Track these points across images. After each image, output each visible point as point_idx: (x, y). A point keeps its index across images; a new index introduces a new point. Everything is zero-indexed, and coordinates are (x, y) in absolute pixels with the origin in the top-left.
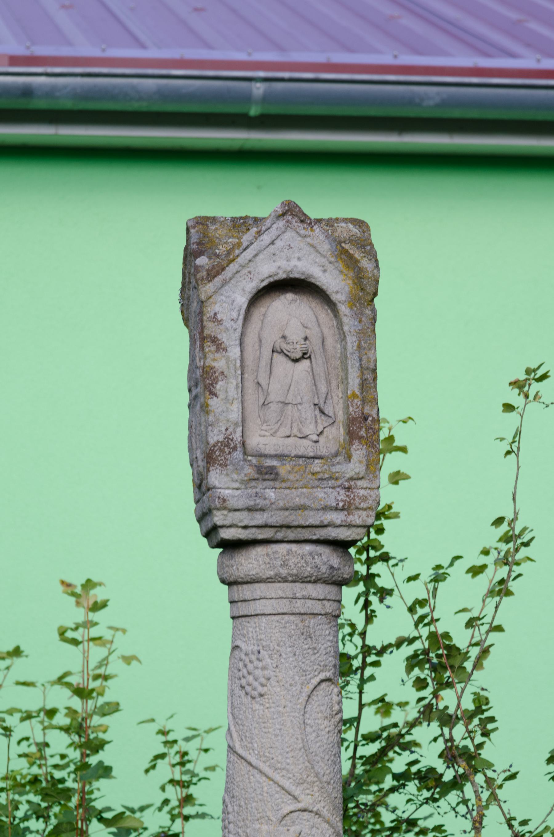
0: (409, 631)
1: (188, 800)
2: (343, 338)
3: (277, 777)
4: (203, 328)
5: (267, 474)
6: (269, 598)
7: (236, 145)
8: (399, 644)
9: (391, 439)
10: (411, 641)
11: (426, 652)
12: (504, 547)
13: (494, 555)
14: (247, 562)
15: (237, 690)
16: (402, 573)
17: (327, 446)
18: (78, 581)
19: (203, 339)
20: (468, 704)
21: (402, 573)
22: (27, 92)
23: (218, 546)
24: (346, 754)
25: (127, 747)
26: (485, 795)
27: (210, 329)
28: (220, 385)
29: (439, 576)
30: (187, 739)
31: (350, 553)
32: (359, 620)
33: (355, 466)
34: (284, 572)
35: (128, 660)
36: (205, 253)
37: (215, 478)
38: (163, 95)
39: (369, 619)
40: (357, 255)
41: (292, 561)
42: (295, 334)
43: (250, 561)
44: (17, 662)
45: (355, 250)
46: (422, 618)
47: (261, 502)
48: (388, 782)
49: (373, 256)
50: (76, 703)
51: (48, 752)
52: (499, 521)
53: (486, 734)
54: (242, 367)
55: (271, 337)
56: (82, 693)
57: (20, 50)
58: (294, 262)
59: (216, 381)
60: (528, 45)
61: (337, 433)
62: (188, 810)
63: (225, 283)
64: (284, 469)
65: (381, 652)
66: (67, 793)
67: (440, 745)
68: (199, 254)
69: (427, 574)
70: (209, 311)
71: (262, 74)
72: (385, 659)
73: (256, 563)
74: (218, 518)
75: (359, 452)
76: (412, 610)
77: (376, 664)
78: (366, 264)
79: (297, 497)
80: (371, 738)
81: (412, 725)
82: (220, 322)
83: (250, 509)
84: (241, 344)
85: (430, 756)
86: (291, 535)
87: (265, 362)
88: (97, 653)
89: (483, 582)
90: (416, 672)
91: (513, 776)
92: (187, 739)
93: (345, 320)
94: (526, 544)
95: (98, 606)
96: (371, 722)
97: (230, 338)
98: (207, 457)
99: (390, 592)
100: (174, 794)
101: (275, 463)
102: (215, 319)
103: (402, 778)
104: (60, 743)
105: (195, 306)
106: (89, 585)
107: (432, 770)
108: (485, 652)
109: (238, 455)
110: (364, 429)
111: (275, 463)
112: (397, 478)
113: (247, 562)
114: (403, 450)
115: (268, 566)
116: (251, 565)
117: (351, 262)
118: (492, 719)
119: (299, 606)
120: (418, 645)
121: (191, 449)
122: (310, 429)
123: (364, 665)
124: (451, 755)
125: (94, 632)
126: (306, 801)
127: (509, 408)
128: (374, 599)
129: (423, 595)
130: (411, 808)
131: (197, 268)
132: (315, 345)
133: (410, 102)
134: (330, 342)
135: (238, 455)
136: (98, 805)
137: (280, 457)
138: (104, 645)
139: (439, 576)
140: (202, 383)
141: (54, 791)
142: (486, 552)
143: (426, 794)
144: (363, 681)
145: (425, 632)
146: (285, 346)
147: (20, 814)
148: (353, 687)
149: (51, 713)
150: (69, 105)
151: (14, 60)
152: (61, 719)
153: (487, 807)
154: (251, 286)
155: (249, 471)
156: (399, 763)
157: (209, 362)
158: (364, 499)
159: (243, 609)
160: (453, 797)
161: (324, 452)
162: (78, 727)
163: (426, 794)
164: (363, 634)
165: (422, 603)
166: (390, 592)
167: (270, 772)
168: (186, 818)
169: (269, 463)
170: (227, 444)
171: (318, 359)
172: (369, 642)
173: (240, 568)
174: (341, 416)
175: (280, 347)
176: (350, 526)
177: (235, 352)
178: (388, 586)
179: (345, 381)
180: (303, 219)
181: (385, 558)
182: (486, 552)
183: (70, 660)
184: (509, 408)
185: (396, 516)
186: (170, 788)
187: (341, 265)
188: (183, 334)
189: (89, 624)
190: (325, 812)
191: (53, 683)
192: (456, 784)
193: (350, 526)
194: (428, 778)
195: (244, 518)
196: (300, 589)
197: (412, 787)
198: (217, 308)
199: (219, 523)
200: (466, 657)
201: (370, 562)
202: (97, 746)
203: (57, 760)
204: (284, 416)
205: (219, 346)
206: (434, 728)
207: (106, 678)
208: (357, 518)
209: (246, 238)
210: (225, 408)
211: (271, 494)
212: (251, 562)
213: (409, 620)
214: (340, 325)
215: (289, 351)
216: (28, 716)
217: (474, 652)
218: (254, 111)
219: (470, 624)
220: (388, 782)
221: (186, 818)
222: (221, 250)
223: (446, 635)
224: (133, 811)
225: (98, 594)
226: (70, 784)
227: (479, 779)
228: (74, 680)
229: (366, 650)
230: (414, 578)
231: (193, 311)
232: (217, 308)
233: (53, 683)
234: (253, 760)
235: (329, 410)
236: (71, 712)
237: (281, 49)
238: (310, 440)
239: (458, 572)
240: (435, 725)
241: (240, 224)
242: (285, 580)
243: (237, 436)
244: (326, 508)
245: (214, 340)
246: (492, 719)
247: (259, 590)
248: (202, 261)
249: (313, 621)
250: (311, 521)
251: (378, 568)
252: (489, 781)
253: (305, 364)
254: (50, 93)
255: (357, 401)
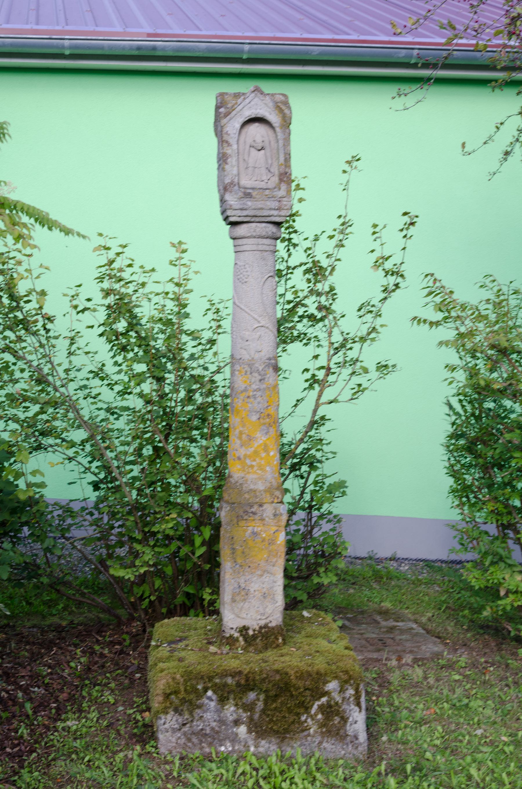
0: (305, 260)
1: (219, 326)
2: (277, 141)
3: (252, 314)
4: (222, 137)
5: (248, 195)
6: (249, 244)
7: (238, 71)
8: (301, 265)
9: (298, 185)
10: (306, 264)
11: (311, 268)
12: (341, 227)
13: (338, 231)
15: (237, 281)
16: (302, 237)
17: (271, 185)
18: (176, 242)
19: (223, 141)
20: (327, 289)
21: (302, 237)
22: (154, 48)
23: (228, 224)
24: (279, 308)
25: (196, 306)
26: (333, 324)
27: (225, 137)
28: (229, 160)
29: (316, 239)
30: (219, 303)
31: (281, 225)
32: (286, 256)
33: (282, 192)
34: (254, 234)
35: (196, 273)
36: (222, 109)
37: (227, 197)
38: (209, 50)
39: (289, 255)
40: (283, 107)
41: (258, 230)
42: (259, 139)
44: (154, 274)
45: (283, 108)
46: (309, 255)
47: (245, 207)
48: (296, 319)
49: (289, 108)
50: (176, 289)
51: (166, 308)
52: (340, 217)
53: (334, 300)
54: (238, 153)
55: (249, 141)
56: (178, 285)
57: (151, 31)
58: (258, 111)
59: (227, 158)
60: (355, 30)
61: (276, 179)
62: (220, 331)
63: (231, 119)
64: (254, 193)
65: (294, 268)
66: (173, 324)
67: (316, 305)
68: (221, 107)
69: (312, 238)
70: (225, 130)
71: (248, 41)
72: (295, 271)
74: (229, 213)
75: (283, 187)
76: (305, 251)
77: (292, 273)
78: (286, 111)
79: (259, 205)
80: (289, 302)
81: (306, 297)
82: (229, 135)
83: (241, 209)
84: (238, 143)
85: (312, 309)
86: (257, 219)
87: (247, 150)
88: (184, 270)
89: (334, 242)
90: (307, 276)
91: (343, 316)
92: (219, 303)
93: (279, 134)
94: (350, 226)
95: (184, 251)
96: (289, 296)
97: (233, 141)
98: (224, 188)
99: (297, 245)
100: (214, 324)
101: (250, 191)
102: (227, 133)
103: (302, 317)
104: (170, 305)
105: (219, 129)
106: (180, 243)
107: (312, 314)
108: (333, 269)
109: (236, 188)
110: (285, 177)
111: (250, 191)
112: (301, 200)
114: (303, 189)
117: (281, 111)
118: (335, 294)
119: (260, 247)
120: (308, 266)
121: (218, 186)
122: (264, 178)
123: (287, 274)
124: (320, 308)
125: (183, 262)
126: (263, 323)
127: (344, 172)
128: (291, 248)
129: (309, 246)
130: (305, 329)
131: (220, 113)
132: (266, 144)
133: (307, 53)
134: (273, 143)
135: (236, 188)
136: (185, 328)
137: (253, 189)
138: (187, 267)
139: (316, 239)
140: (222, 159)
141: (169, 323)
142: (335, 230)
143: (311, 323)
144: (287, 280)
145: (311, 260)
146: (255, 145)
147: (155, 332)
148: (283, 282)
149: (167, 293)
150: (171, 54)
151: (149, 35)
152: (171, 296)
153: (333, 327)
154: (242, 120)
155: (241, 194)
156: (301, 311)
157: (225, 151)
158: (286, 205)
159: (239, 249)
160: (321, 324)
161: (270, 187)
162: (177, 299)
163: (311, 323)
164: (287, 261)
165: (310, 249)
166: (297, 245)
167: (249, 312)
168: (219, 334)
169: (248, 191)
170: (232, 183)
171: (268, 150)
172: (290, 264)
174: (277, 173)
176: (280, 216)
177: (235, 147)
178: (297, 242)
179: (278, 158)
180: (262, 93)
181: (296, 232)
182: (335, 230)
183: (174, 272)
184: (344, 172)
185: (300, 215)
186: (212, 322)
187: (277, 112)
188: (214, 141)
189: (181, 258)
190: (270, 327)
191: (168, 282)
192: (322, 319)
193: (280, 216)
194: (311, 317)
195: (239, 213)
196: (261, 241)
197: (305, 320)
198: (228, 129)
200: (326, 269)
201: (290, 233)
202: (185, 306)
203: (169, 312)
204: (255, 174)
205: (229, 145)
206: (313, 298)
207: (188, 280)
208: (283, 213)
209: (239, 101)
210: (231, 169)
211: (249, 203)
212: (241, 230)
213: (305, 255)
214: (277, 136)
216: (157, 294)
217: (329, 269)
218: (245, 57)
219: (328, 257)
220: (296, 319)
221: (219, 334)
222: (229, 105)
223: (318, 262)
224: (198, 331)
225: (184, 247)
226: (174, 321)
227: (331, 317)
228: (176, 280)
229: (288, 268)
230: (306, 239)
231: (219, 131)
232: (228, 129)
233: (168, 282)
234: (242, 307)
235: (272, 170)
236: (174, 293)
237: (256, 31)
239: (324, 238)
240: (314, 296)
241: (237, 96)
242: (255, 237)
243: (236, 180)
244: (271, 209)
245: (227, 142)
246: (335, 294)
247: (244, 241)
248: (222, 110)
249: (265, 254)
251: (292, 236)
252: (335, 318)
253: (262, 152)
254: (164, 49)
255: (283, 167)
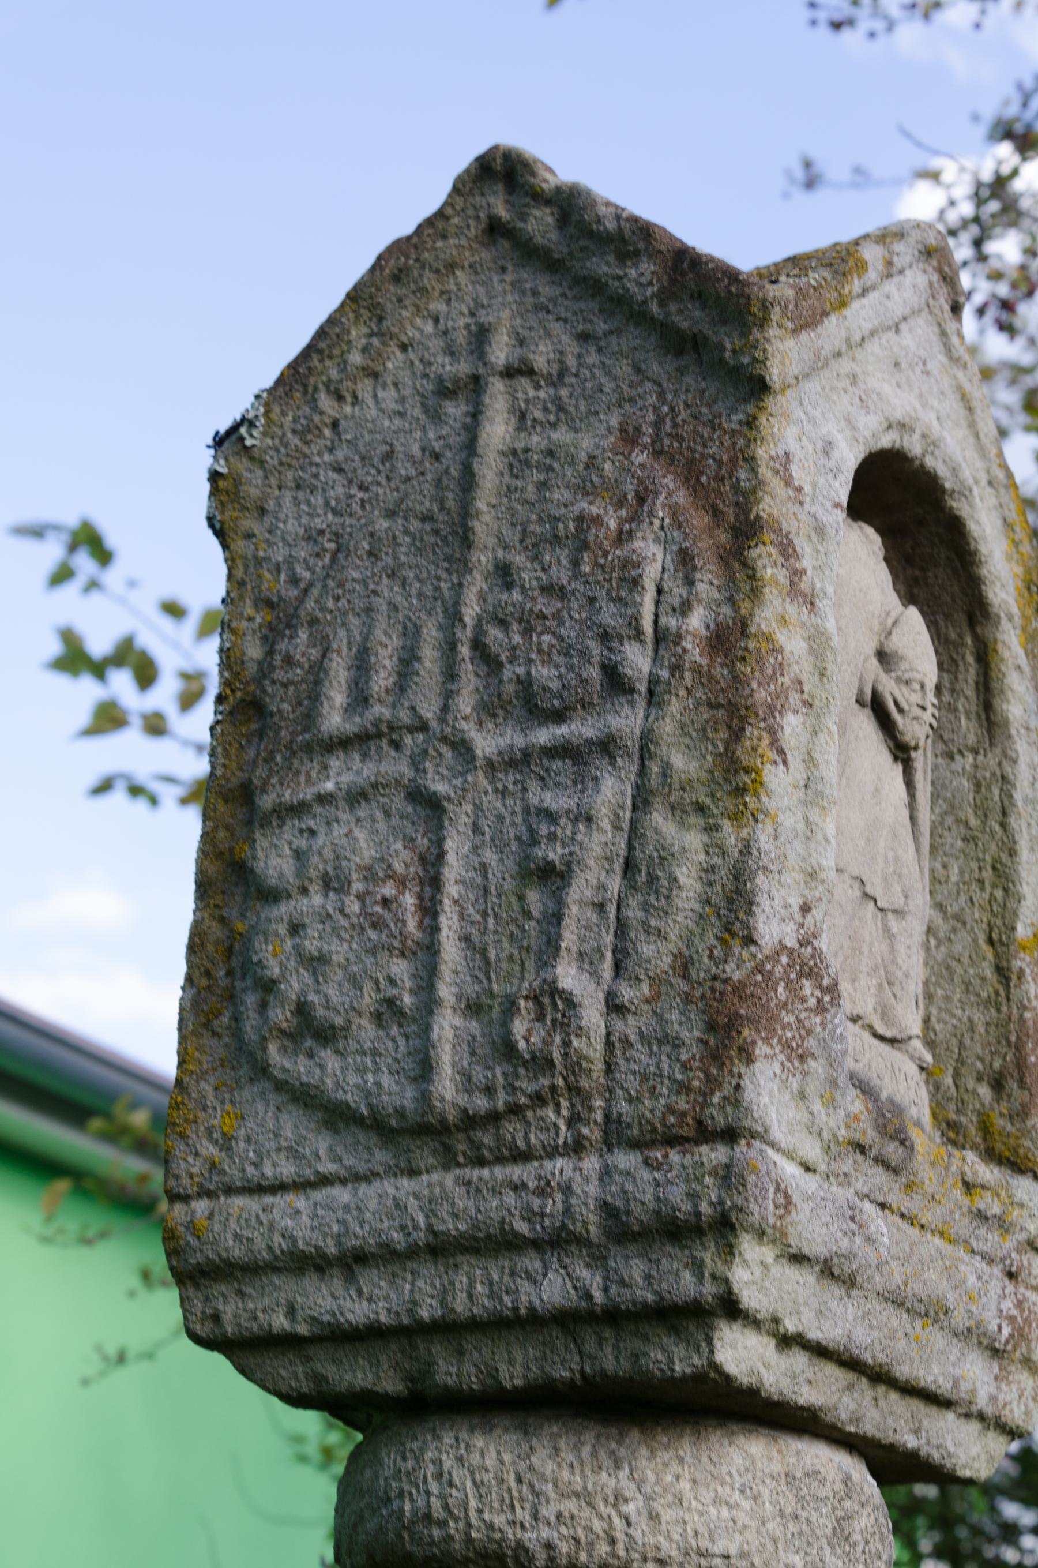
14: (707, 1496)
43: (724, 1491)
73: (746, 1504)
113: (707, 1496)
115: (792, 1527)
116: (725, 1513)
173: (666, 1515)
175: (875, 681)
199: (750, 1298)
215: (900, 710)
238: (912, 1058)
250: (933, 1375)
